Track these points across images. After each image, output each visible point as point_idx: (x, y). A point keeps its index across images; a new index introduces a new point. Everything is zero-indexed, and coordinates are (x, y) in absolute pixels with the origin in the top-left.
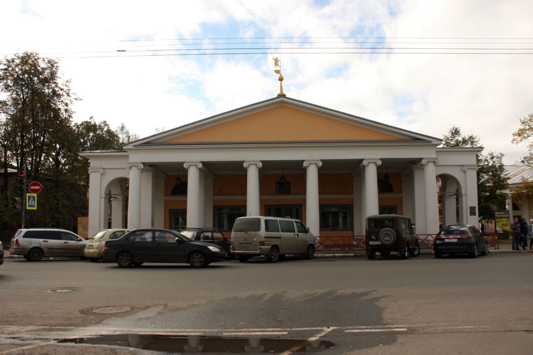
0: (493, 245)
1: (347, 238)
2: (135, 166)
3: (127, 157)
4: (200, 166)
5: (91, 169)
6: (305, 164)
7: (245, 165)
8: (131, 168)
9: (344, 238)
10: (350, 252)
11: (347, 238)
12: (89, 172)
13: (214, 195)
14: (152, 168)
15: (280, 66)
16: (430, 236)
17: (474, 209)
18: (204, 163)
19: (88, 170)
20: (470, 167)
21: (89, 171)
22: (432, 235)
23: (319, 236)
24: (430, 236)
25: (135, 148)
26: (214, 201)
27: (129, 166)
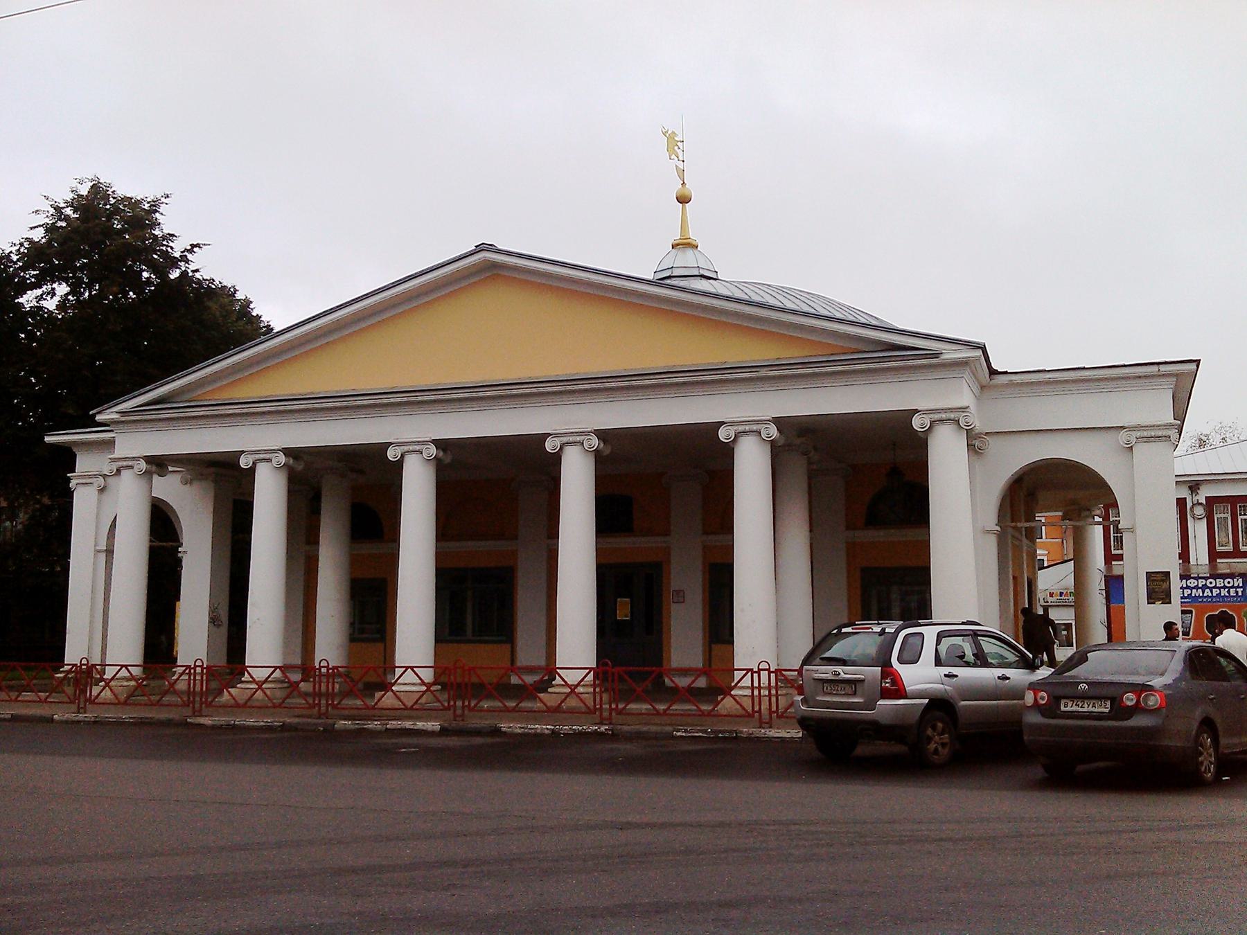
1: (764, 675)
2: (575, 443)
3: (110, 444)
5: (79, 477)
6: (549, 446)
7: (244, 462)
8: (119, 471)
9: (756, 675)
10: (205, 710)
11: (764, 675)
12: (71, 485)
13: (706, 533)
14: (212, 470)
15: (681, 159)
17: (1163, 581)
18: (602, 434)
19: (69, 479)
20: (1145, 434)
21: (72, 484)
22: (129, 668)
23: (432, 665)
25: (123, 419)
26: (706, 549)
27: (114, 466)
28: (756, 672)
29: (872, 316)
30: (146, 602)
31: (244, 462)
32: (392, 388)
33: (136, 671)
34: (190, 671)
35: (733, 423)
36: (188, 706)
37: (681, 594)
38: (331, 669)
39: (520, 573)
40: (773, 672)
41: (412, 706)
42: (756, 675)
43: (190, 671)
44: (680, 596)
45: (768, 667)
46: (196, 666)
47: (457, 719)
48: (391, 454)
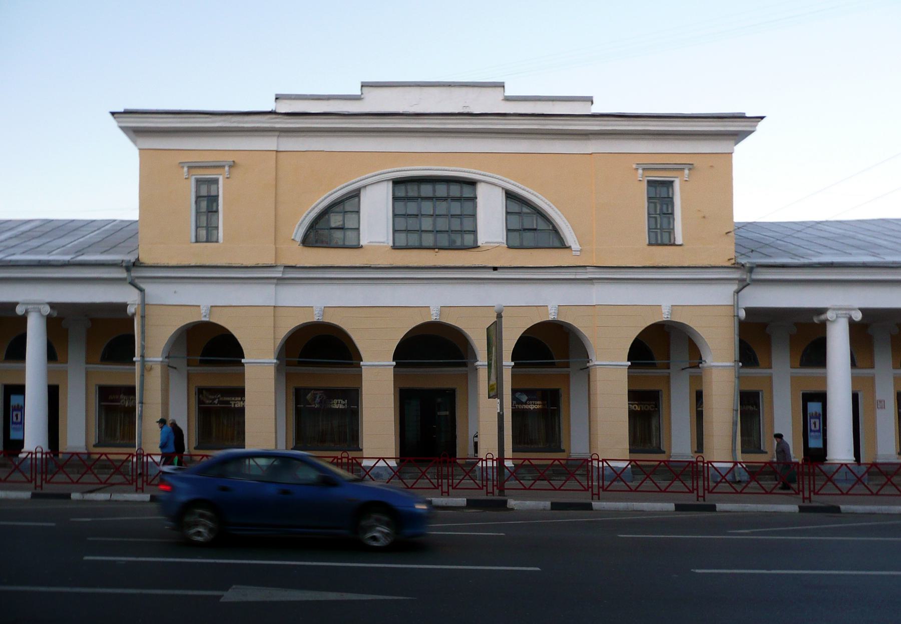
0: (799, 491)
4: (47, 310)
9: (484, 462)
16: (739, 491)
18: (53, 305)
24: (739, 491)
28: (484, 460)
29: (443, 170)
30: (3, 416)
31: (20, 310)
32: (336, 215)
33: (393, 463)
34: (693, 465)
35: (24, 304)
36: (482, 489)
37: (883, 403)
38: (350, 459)
39: (876, 377)
40: (495, 460)
41: (665, 490)
42: (484, 462)
43: (693, 465)
44: (882, 404)
45: (702, 460)
46: (36, 453)
47: (489, 495)
48: (20, 310)
